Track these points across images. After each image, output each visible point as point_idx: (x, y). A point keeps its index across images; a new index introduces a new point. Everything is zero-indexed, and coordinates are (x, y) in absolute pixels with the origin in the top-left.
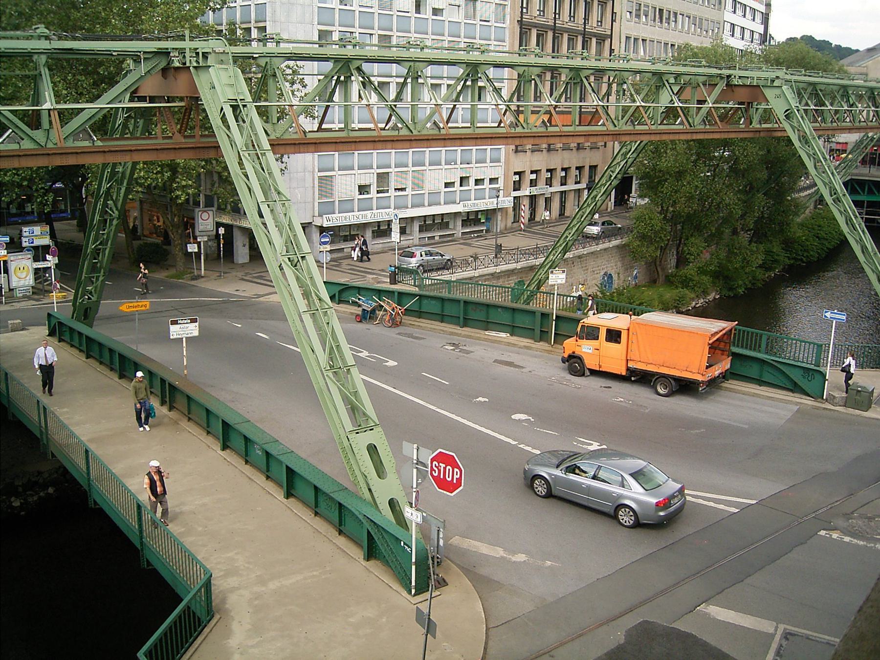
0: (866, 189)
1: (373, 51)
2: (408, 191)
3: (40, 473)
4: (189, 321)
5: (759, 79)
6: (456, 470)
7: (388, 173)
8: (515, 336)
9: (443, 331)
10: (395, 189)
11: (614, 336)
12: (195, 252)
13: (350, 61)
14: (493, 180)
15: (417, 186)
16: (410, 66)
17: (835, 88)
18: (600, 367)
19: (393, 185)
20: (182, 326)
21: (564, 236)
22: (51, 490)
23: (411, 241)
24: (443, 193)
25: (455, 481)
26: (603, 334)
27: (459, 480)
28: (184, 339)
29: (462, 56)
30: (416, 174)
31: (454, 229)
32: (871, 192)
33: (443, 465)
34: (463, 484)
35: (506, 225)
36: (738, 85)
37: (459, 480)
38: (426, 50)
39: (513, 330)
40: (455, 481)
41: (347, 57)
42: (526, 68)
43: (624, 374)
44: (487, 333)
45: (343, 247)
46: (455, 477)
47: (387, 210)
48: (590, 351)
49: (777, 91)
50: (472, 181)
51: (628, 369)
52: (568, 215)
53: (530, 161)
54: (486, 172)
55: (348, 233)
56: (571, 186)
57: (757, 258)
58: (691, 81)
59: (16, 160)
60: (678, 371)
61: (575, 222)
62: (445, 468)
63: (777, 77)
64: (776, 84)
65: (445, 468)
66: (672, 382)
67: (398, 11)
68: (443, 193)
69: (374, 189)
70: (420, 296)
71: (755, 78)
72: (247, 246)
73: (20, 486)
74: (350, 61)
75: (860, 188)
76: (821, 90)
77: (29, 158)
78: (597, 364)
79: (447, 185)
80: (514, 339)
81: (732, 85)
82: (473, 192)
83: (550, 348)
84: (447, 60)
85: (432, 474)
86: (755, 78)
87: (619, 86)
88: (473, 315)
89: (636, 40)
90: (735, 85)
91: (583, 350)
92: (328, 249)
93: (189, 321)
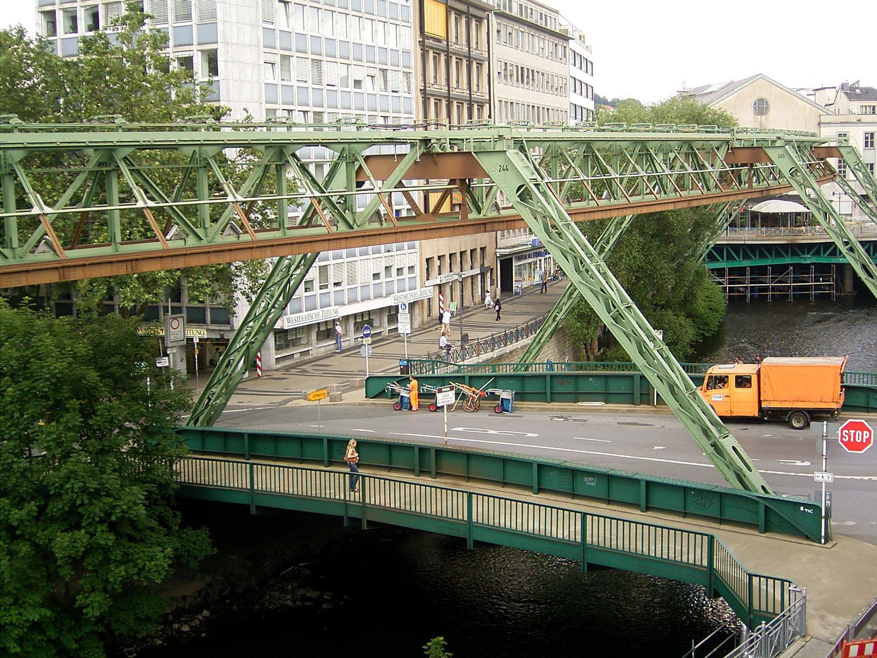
0: (725, 255)
1: (310, 134)
2: (345, 286)
3: (184, 598)
4: (449, 389)
5: (477, 140)
6: (865, 432)
7: (326, 266)
8: (610, 403)
9: (531, 408)
10: (334, 284)
11: (742, 381)
12: (165, 367)
13: (284, 147)
14: (411, 268)
15: (352, 280)
16: (194, 151)
17: (624, 145)
18: (731, 412)
19: (332, 280)
20: (445, 393)
21: (553, 316)
22: (206, 613)
23: (348, 342)
24: (372, 287)
25: (864, 441)
26: (732, 381)
27: (868, 440)
28: (445, 407)
29: (261, 134)
30: (349, 264)
31: (380, 326)
32: (730, 258)
33: (852, 432)
34: (872, 442)
35: (423, 321)
36: (442, 153)
37: (868, 440)
38: (294, 129)
39: (607, 397)
40: (864, 441)
41: (139, 144)
42: (197, 148)
43: (757, 415)
44: (580, 404)
45: (294, 352)
46: (865, 437)
47: (328, 308)
48: (721, 399)
49: (780, 151)
50: (406, 270)
51: (760, 409)
52: (467, 305)
53: (437, 246)
54: (405, 262)
55: (294, 338)
56: (468, 273)
57: (687, 332)
58: (612, 149)
59: (182, 259)
60: (813, 404)
61: (565, 299)
62: (855, 434)
63: (779, 138)
64: (778, 143)
65: (855, 434)
66: (807, 414)
67: (393, 91)
68: (372, 287)
69: (383, 275)
70: (496, 377)
71: (472, 140)
72: (185, 361)
73: (169, 614)
74: (284, 147)
75: (735, 253)
76: (598, 150)
77: (35, 274)
78: (729, 410)
79: (376, 276)
80: (611, 406)
81: (433, 154)
82: (396, 282)
83: (654, 409)
84: (247, 142)
85: (842, 441)
86: (472, 140)
87: (665, 156)
88: (559, 388)
89: (548, 109)
90: (438, 154)
91: (713, 399)
92: (370, 342)
93: (449, 389)
